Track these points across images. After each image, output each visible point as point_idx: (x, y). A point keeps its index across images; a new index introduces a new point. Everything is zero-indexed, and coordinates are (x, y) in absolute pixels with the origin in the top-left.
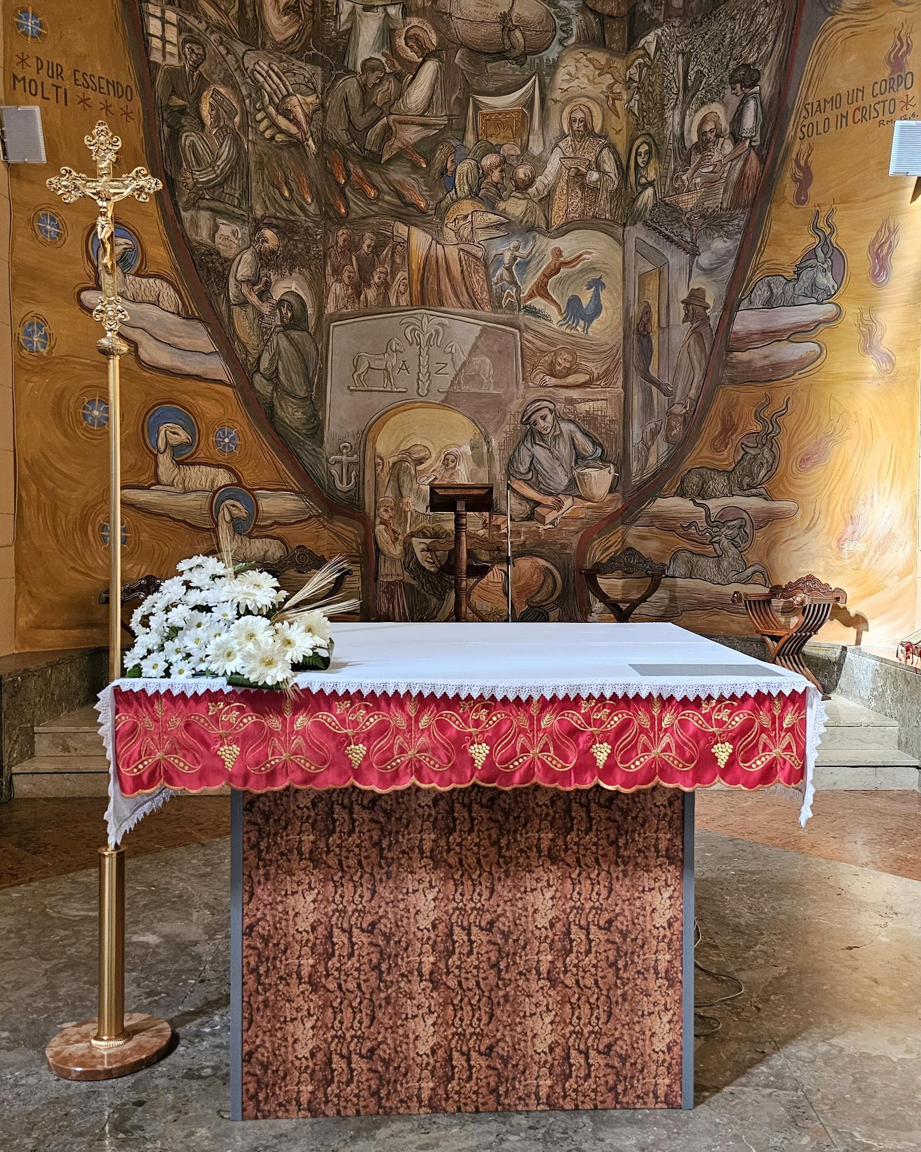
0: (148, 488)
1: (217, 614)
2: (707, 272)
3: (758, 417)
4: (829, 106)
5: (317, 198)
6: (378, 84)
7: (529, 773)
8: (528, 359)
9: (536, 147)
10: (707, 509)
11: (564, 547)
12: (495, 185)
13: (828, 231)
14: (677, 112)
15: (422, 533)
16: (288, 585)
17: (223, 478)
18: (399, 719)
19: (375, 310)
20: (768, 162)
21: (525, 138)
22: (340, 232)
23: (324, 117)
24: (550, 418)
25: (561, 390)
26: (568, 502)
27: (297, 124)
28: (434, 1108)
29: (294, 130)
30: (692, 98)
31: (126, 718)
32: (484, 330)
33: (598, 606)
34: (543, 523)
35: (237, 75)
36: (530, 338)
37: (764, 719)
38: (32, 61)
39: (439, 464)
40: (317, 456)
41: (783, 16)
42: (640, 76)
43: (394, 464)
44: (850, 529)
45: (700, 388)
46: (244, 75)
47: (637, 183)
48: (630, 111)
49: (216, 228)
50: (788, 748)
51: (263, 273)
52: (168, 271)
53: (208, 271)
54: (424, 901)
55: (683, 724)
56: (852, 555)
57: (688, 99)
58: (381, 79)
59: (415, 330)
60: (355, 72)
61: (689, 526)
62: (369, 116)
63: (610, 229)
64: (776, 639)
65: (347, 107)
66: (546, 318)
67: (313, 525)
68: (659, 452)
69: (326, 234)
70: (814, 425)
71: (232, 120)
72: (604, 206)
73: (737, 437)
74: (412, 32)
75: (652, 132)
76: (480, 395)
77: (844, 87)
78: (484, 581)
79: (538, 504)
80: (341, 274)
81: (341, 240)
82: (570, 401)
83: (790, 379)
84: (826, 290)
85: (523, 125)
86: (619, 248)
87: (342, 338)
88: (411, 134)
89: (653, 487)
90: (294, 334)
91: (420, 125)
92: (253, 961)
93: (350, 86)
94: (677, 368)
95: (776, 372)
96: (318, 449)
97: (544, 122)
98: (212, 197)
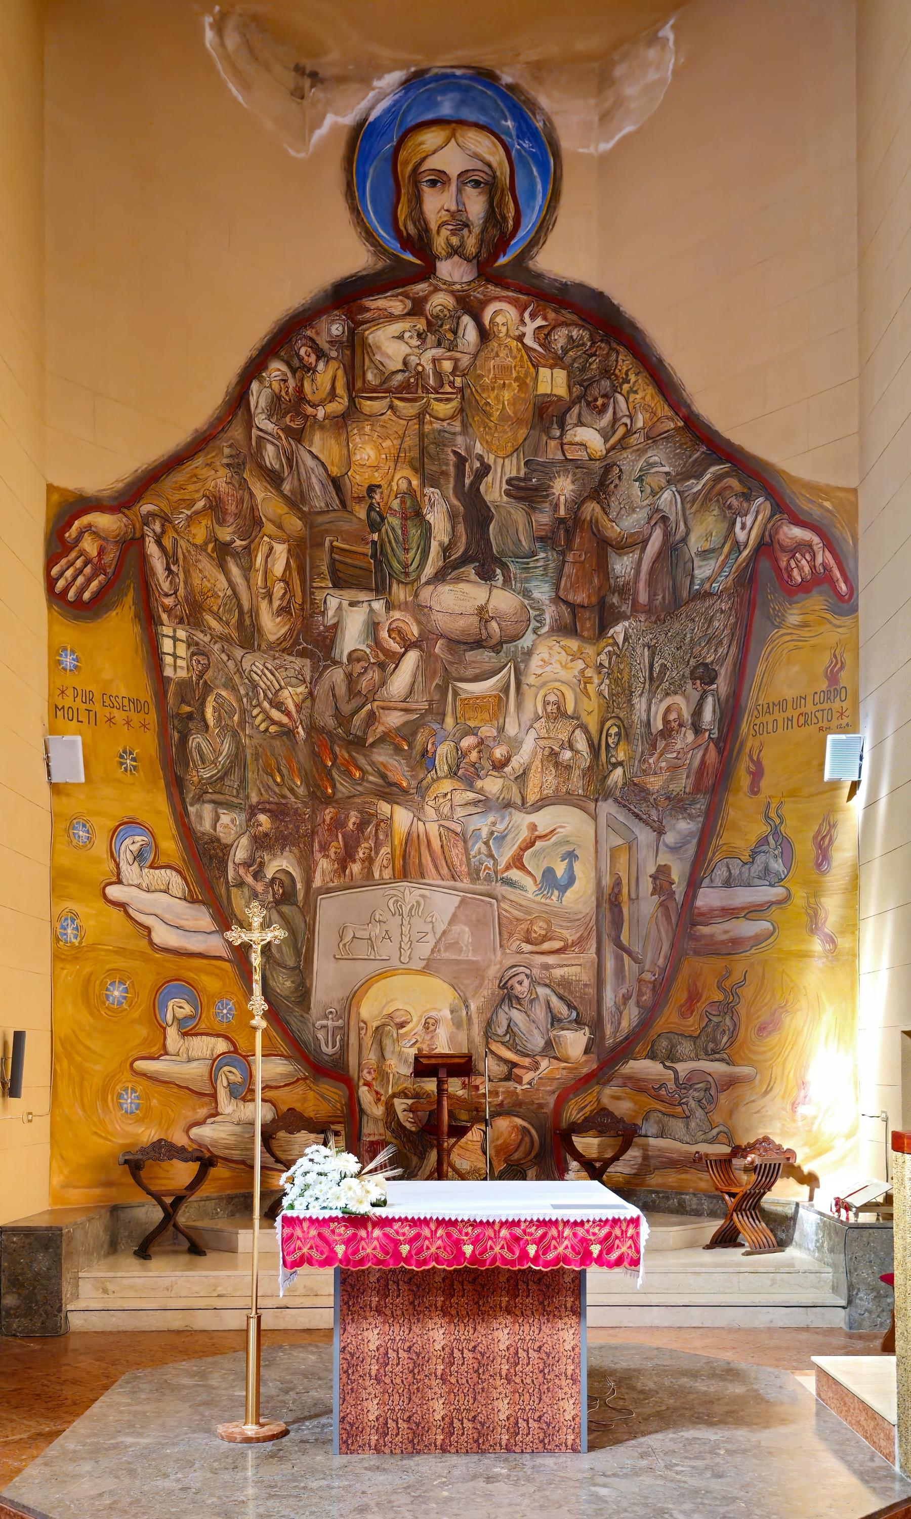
0: (157, 1059)
1: (330, 1176)
2: (674, 849)
3: (720, 987)
4: (776, 708)
5: (306, 781)
6: (363, 674)
7: (494, 1260)
8: (505, 927)
9: (511, 729)
10: (676, 1072)
11: (541, 1106)
12: (473, 765)
13: (778, 821)
14: (644, 700)
15: (404, 1094)
16: (362, 1161)
17: (222, 1046)
18: (426, 1232)
19: (359, 883)
20: (726, 753)
21: (501, 720)
22: (328, 811)
23: (313, 705)
24: (526, 982)
25: (537, 957)
26: (544, 1063)
27: (288, 714)
28: (444, 1450)
29: (285, 720)
30: (658, 688)
31: (288, 1231)
32: (463, 901)
33: (574, 1165)
34: (520, 1083)
35: (236, 678)
36: (507, 908)
37: (617, 1231)
38: (70, 692)
39: (420, 1027)
40: (304, 1021)
41: (736, 623)
42: (610, 663)
43: (377, 1028)
44: (802, 1093)
45: (668, 958)
46: (241, 677)
47: (608, 762)
48: (600, 694)
49: (217, 819)
50: (630, 1247)
51: (257, 854)
52: (179, 863)
53: (211, 858)
54: (437, 1335)
55: (575, 1235)
56: (804, 1118)
57: (654, 687)
58: (366, 669)
59: (397, 901)
60: (340, 663)
61: (660, 1088)
62: (354, 703)
63: (581, 803)
64: (732, 1195)
65: (334, 695)
66: (522, 888)
67: (300, 1089)
68: (631, 1017)
69: (313, 812)
70: (768, 997)
71: (231, 718)
72: (576, 783)
73: (701, 1006)
74: (394, 626)
75: (621, 715)
76: (458, 962)
77: (789, 693)
78: (463, 1140)
79: (515, 1065)
80: (328, 850)
81: (328, 818)
82: (546, 967)
83: (748, 954)
84: (777, 874)
85: (499, 709)
86: (592, 822)
87: (329, 911)
88: (394, 719)
89: (625, 1049)
90: (285, 909)
91: (402, 710)
92: (345, 1366)
93: (337, 676)
94: (647, 936)
95: (736, 944)
96: (305, 1015)
97: (519, 705)
98: (216, 791)
